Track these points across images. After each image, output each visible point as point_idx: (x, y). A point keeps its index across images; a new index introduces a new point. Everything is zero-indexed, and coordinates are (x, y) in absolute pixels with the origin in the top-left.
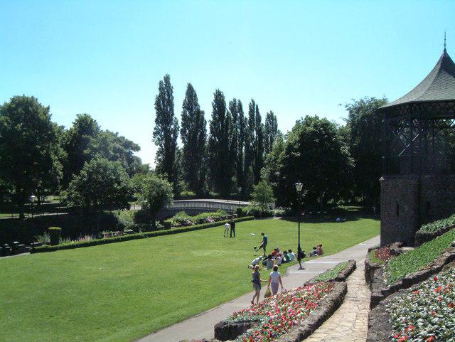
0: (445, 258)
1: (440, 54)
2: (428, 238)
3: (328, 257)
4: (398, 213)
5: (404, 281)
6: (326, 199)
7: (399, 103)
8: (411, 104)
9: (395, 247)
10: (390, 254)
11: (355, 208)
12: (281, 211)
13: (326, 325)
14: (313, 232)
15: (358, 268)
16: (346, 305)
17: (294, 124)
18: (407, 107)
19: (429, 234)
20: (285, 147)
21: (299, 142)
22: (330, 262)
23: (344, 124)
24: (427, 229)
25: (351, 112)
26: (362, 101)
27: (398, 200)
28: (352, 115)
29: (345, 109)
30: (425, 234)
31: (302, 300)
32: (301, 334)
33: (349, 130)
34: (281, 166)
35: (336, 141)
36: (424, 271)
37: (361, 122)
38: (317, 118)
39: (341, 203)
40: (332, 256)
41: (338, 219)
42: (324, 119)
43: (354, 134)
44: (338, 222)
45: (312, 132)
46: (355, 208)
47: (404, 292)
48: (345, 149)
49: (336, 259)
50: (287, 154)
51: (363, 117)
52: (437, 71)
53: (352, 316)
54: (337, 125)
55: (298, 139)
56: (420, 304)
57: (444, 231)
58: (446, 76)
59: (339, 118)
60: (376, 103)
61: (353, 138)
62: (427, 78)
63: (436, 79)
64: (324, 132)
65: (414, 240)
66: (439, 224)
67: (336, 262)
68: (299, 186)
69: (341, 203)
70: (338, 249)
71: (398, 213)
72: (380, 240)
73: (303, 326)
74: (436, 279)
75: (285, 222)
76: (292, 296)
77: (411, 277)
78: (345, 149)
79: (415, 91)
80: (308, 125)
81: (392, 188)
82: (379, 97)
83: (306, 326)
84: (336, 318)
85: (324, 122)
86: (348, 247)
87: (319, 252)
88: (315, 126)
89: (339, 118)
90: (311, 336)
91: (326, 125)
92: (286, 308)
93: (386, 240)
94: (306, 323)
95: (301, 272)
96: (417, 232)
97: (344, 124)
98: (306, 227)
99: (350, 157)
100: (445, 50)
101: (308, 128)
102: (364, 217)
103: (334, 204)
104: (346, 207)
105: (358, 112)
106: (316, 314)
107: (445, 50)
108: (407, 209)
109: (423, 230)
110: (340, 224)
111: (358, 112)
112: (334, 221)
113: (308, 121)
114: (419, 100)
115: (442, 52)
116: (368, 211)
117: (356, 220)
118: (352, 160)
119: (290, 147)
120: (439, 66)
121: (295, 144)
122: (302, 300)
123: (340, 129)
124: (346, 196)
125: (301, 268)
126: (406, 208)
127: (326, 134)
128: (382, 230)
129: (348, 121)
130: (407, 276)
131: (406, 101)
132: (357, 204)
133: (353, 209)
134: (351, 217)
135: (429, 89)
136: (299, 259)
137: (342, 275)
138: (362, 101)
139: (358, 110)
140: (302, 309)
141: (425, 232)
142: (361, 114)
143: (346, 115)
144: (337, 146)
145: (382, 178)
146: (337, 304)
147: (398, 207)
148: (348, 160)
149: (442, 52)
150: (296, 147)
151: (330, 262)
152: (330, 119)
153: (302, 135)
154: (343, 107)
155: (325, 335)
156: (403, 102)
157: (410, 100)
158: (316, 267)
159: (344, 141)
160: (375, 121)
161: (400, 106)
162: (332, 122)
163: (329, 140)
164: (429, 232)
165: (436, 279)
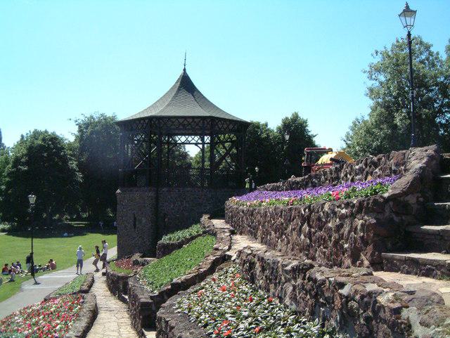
0: (210, 261)
2: (168, 249)
3: (61, 271)
4: (135, 225)
5: (173, 285)
8: (151, 119)
9: (137, 257)
11: (82, 224)
12: (7, 226)
14: (45, 248)
15: (96, 280)
16: (102, 315)
17: (19, 139)
18: (147, 121)
20: (11, 161)
21: (26, 155)
22: (66, 276)
23: (72, 139)
24: (170, 239)
25: (80, 127)
26: (92, 117)
28: (80, 131)
29: (75, 124)
31: (52, 313)
34: (7, 179)
35: (65, 155)
38: (46, 132)
39: (67, 219)
41: (66, 234)
42: (53, 133)
44: (65, 237)
45: (40, 145)
46: (82, 224)
48: (73, 164)
50: (13, 167)
51: (92, 133)
52: (176, 89)
53: (114, 326)
54: (66, 139)
55: (25, 152)
56: (18, 330)
57: (188, 241)
59: (68, 133)
61: (81, 154)
63: (179, 90)
64: (52, 146)
65: (154, 250)
66: (185, 233)
68: (32, 199)
71: (135, 225)
72: (116, 253)
74: (214, 280)
75: (11, 237)
76: (38, 310)
79: (154, 106)
80: (37, 139)
81: (132, 201)
82: (109, 114)
84: (96, 328)
87: (52, 267)
88: (44, 140)
89: (68, 133)
91: (54, 140)
92: (37, 322)
95: (37, 287)
96: (160, 242)
97: (72, 139)
98: (38, 242)
100: (185, 70)
101: (36, 142)
102: (92, 232)
103: (60, 220)
105: (87, 128)
107: (185, 70)
108: (144, 221)
109: (165, 240)
110: (66, 239)
111: (87, 128)
113: (36, 134)
115: (182, 71)
119: (17, 161)
120: (179, 83)
121: (22, 157)
122: (52, 313)
123: (68, 144)
125: (36, 283)
127: (56, 147)
129: (77, 137)
132: (83, 220)
134: (79, 232)
135: (168, 105)
136: (33, 275)
137: (85, 288)
138: (92, 117)
139: (87, 125)
140: (58, 322)
141: (168, 242)
142: (90, 130)
143: (75, 130)
144: (65, 160)
145: (118, 191)
146: (94, 314)
147: (135, 218)
150: (23, 160)
151: (66, 276)
152: (58, 134)
153: (30, 149)
154: (73, 122)
156: (142, 116)
158: (53, 282)
159: (71, 155)
163: (57, 154)
164: (171, 242)
165: (214, 280)
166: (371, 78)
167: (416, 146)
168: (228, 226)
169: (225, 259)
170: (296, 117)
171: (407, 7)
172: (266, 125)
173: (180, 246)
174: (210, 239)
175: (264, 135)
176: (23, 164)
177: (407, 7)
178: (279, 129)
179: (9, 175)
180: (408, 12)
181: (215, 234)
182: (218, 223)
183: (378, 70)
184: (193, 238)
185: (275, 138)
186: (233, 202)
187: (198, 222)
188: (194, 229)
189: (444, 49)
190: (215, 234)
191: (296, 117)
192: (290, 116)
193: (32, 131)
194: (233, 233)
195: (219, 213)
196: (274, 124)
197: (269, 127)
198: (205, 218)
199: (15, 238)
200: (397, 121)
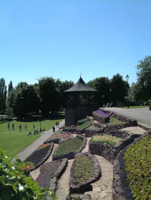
21: (22, 93)
25: (40, 82)
26: (44, 78)
48: (38, 96)
55: (21, 92)
57: (86, 121)
58: (81, 84)
63: (79, 84)
66: (82, 121)
78: (38, 96)
82: (50, 77)
109: (79, 121)
138: (44, 78)
139: (42, 81)
154: (37, 80)
166: (138, 69)
167: (78, 125)
168: (93, 118)
169: (92, 124)
170: (118, 75)
171: (127, 75)
172: (107, 78)
173: (83, 123)
174: (90, 121)
175: (106, 82)
176: (22, 96)
177: (127, 75)
178: (112, 79)
179: (16, 100)
180: (127, 76)
181: (90, 120)
182: (91, 118)
183: (140, 67)
184: (86, 121)
185: (110, 83)
186: (94, 113)
187: (86, 117)
188: (85, 119)
189: (131, 83)
190: (90, 120)
191: (118, 75)
192: (116, 75)
193: (20, 82)
194: (94, 120)
195: (91, 115)
196: (110, 77)
197: (108, 78)
198: (88, 116)
199: (20, 122)
200: (145, 84)
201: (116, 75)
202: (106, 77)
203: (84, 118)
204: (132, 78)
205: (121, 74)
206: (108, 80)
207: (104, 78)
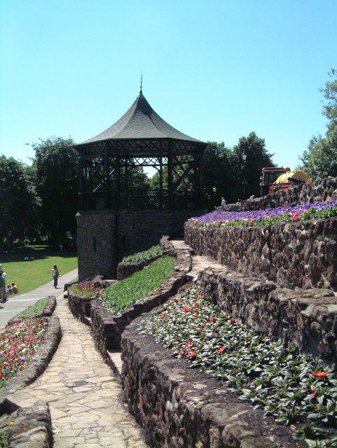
1: (134, 97)
3: (24, 295)
6: (12, 239)
7: (96, 140)
8: (108, 142)
9: (98, 279)
10: (95, 287)
11: (42, 247)
13: (56, 357)
16: (66, 338)
19: (133, 266)
23: (30, 164)
24: (131, 261)
25: (38, 151)
27: (95, 234)
28: (38, 155)
30: (129, 266)
31: (16, 337)
32: (38, 370)
33: (35, 169)
36: (154, 297)
37: (47, 162)
39: (27, 243)
40: (29, 294)
41: (26, 258)
42: (12, 158)
43: (40, 173)
44: (26, 260)
46: (42, 247)
47: (145, 315)
48: (32, 189)
49: (32, 297)
51: (50, 157)
53: (78, 348)
54: (24, 164)
57: (153, 259)
58: (141, 115)
60: (62, 143)
62: (129, 111)
63: (133, 117)
64: (10, 171)
65: (113, 272)
67: (34, 300)
69: (27, 243)
70: (32, 287)
73: (36, 361)
74: (176, 301)
77: (142, 303)
78: (32, 189)
81: (92, 223)
82: (66, 138)
83: (40, 360)
85: (11, 161)
86: (42, 284)
89: (26, 158)
90: (47, 370)
91: (13, 164)
93: (85, 275)
94: (38, 358)
97: (30, 164)
99: (37, 196)
100: (141, 92)
103: (19, 244)
104: (33, 246)
105: (44, 152)
106: (48, 347)
107: (141, 92)
109: (126, 261)
110: (29, 263)
111: (44, 152)
112: (23, 260)
114: (117, 137)
115: (139, 94)
116: (56, 248)
117: (44, 258)
118: (39, 199)
120: (135, 106)
124: (32, 234)
126: (104, 243)
127: (14, 172)
128: (79, 266)
129: (35, 161)
130: (137, 302)
131: (103, 138)
132: (43, 243)
133: (40, 247)
134: (39, 255)
135: (126, 128)
137: (48, 311)
138: (49, 141)
139: (45, 149)
140: (24, 345)
141: (128, 263)
142: (47, 154)
143: (33, 154)
144: (23, 184)
145: (78, 214)
146: (59, 336)
148: (35, 199)
149: (138, 94)
152: (16, 159)
154: (30, 146)
155: (61, 368)
157: (107, 137)
159: (30, 180)
160: (61, 162)
161: (97, 143)
162: (19, 161)
163: (16, 179)
164: (132, 264)
165: (176, 301)
166: (327, 97)
169: (186, 280)
170: (253, 136)
172: (223, 145)
173: (140, 267)
174: (170, 260)
175: (221, 155)
178: (236, 148)
181: (175, 256)
182: (178, 244)
184: (153, 259)
185: (232, 157)
186: (193, 223)
187: (157, 243)
188: (154, 251)
190: (175, 256)
191: (253, 136)
194: (193, 253)
195: (178, 234)
196: (231, 143)
197: (225, 146)
198: (164, 239)
201: (247, 136)
202: (219, 142)
203: (147, 248)
204: (289, 153)
205: (260, 135)
206: (225, 150)
207: (216, 143)
